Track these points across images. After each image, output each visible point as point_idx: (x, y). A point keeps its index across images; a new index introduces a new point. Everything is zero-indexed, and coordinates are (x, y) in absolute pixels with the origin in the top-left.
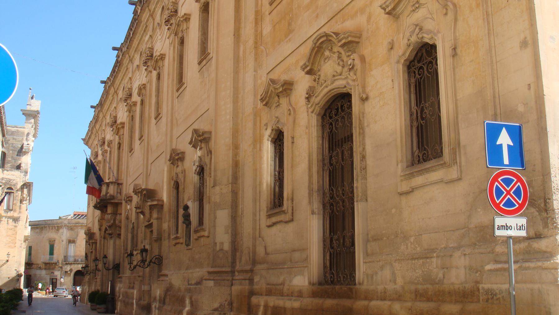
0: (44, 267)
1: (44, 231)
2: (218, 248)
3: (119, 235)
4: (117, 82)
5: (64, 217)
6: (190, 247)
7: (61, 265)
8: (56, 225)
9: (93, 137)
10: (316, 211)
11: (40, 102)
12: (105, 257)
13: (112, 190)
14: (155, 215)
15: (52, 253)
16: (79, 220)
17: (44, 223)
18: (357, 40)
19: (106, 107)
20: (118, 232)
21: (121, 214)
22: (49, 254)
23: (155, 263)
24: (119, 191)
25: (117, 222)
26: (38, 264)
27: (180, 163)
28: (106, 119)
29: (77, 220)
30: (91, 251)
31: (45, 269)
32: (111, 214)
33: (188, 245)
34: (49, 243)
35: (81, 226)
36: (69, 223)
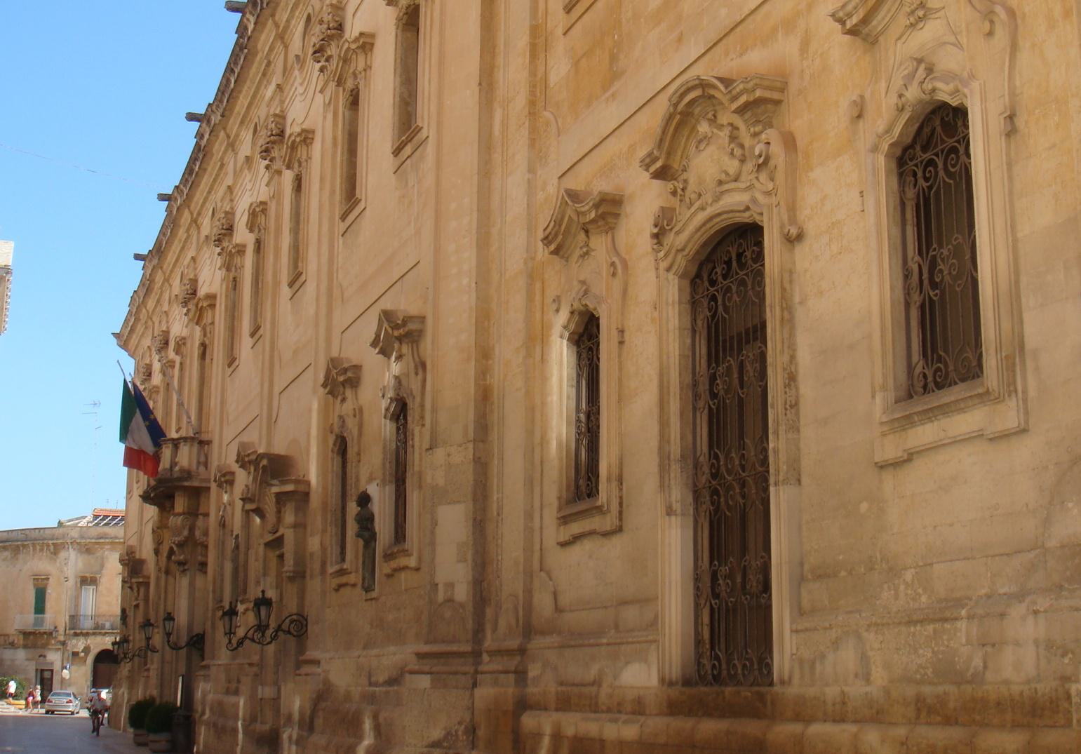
0: (21, 642)
1: (21, 557)
2: (441, 597)
3: (204, 565)
4: (199, 196)
5: (69, 521)
6: (374, 594)
7: (62, 638)
8: (51, 542)
9: (140, 328)
10: (677, 507)
11: (12, 244)
12: (170, 617)
13: (186, 457)
14: (289, 518)
15: (40, 608)
16: (107, 529)
17: (21, 536)
18: (776, 96)
19: (171, 258)
20: (200, 558)
21: (207, 515)
22: (33, 610)
23: (289, 632)
24: (202, 459)
25: (197, 533)
26: (8, 635)
27: (349, 393)
28: (171, 286)
29: (102, 530)
30: (135, 603)
31: (25, 647)
32: (184, 514)
33: (368, 589)
34: (35, 585)
35: (111, 543)
36: (82, 537)
